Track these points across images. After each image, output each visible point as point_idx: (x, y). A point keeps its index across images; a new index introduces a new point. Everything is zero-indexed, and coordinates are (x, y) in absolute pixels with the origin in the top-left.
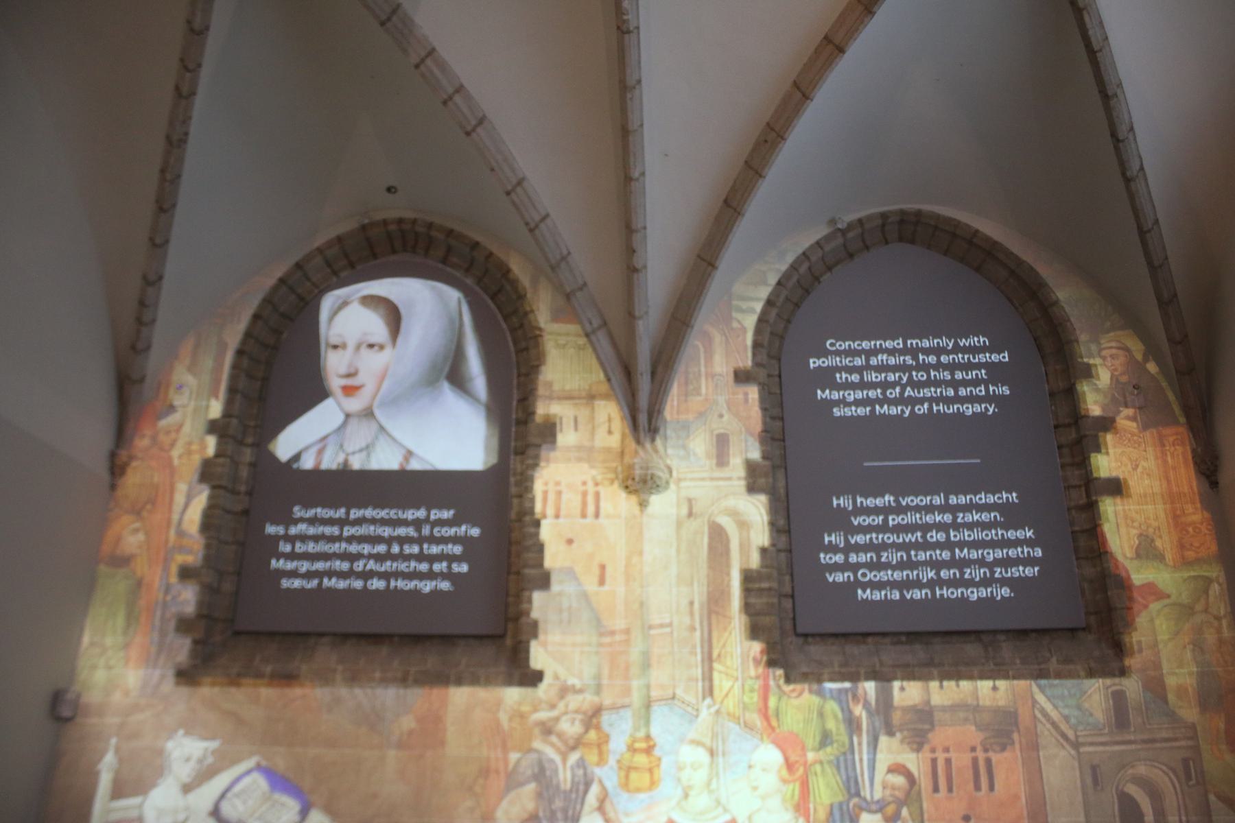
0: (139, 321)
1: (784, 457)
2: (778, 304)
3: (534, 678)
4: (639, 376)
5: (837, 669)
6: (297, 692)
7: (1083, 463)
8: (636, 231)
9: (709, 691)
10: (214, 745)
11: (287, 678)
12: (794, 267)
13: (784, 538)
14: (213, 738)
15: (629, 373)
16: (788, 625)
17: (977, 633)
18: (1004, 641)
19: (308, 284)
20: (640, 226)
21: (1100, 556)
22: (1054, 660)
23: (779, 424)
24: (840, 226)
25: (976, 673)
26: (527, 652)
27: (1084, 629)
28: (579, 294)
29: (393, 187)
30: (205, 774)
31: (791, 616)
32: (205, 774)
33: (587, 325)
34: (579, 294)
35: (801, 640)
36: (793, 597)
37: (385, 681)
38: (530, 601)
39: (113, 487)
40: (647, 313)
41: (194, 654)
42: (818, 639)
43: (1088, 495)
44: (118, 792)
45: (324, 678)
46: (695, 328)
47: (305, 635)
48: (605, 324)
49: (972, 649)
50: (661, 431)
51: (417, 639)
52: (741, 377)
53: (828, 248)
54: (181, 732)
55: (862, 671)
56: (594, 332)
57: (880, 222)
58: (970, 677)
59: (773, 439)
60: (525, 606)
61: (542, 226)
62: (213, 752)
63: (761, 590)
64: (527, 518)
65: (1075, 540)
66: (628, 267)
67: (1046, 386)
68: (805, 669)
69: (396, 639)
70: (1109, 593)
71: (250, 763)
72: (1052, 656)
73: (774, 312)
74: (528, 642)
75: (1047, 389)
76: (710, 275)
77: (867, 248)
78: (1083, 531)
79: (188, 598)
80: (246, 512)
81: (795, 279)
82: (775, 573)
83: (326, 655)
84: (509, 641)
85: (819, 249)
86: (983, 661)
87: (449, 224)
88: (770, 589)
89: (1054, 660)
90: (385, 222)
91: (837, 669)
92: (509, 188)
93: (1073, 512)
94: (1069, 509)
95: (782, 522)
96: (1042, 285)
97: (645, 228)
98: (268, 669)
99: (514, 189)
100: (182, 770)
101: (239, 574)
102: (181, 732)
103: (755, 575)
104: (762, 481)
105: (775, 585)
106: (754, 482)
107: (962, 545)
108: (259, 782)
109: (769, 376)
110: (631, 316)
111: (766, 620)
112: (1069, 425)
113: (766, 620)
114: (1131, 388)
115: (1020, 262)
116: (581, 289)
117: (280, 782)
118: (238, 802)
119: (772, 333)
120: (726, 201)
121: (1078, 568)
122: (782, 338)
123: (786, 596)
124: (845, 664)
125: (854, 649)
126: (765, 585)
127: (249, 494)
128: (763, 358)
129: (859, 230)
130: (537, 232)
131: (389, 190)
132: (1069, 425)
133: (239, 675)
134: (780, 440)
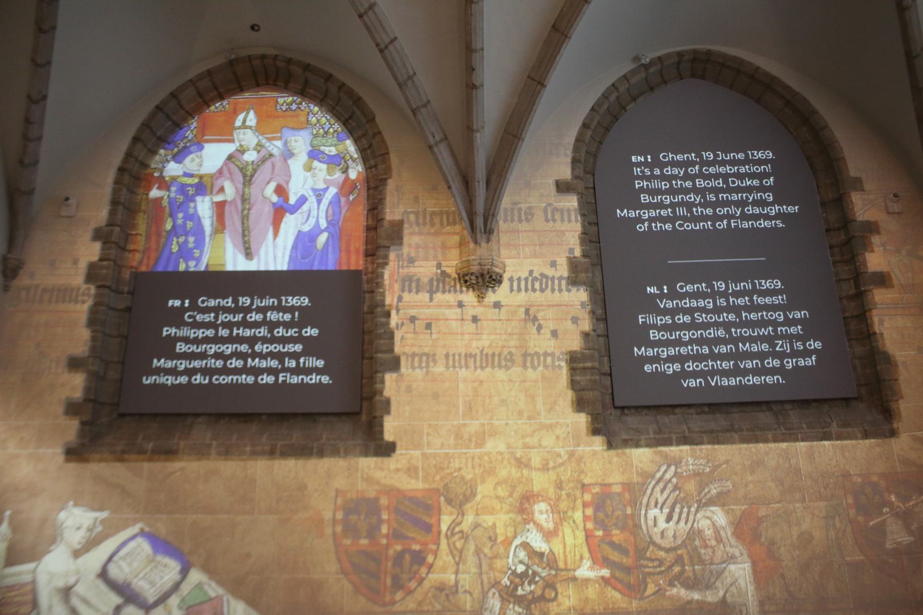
0: (26, 138)
2: (593, 127)
3: (387, 450)
4: (476, 183)
5: (652, 436)
6: (178, 465)
8: (476, 51)
10: (104, 515)
11: (170, 453)
12: (605, 96)
13: (602, 325)
14: (101, 509)
15: (467, 182)
16: (608, 398)
17: (767, 403)
18: (791, 410)
19: (183, 112)
20: (479, 46)
21: (869, 335)
22: (834, 423)
23: (594, 228)
24: (643, 62)
25: (770, 436)
26: (382, 426)
27: (856, 399)
28: (423, 110)
29: (258, 26)
30: (91, 544)
31: (610, 391)
32: (91, 544)
33: (431, 138)
34: (423, 110)
35: (619, 412)
36: (611, 375)
37: (254, 454)
38: (383, 382)
40: (483, 127)
41: (82, 434)
42: (633, 411)
43: (857, 286)
45: (201, 452)
46: (527, 139)
47: (186, 415)
48: (446, 138)
49: (764, 417)
50: (496, 231)
51: (283, 417)
52: (562, 187)
53: (633, 81)
54: (71, 503)
56: (436, 144)
58: (766, 441)
59: (591, 241)
60: (378, 386)
61: (391, 47)
62: (103, 522)
63: (584, 369)
66: (467, 85)
67: (818, 196)
68: (625, 436)
69: (264, 417)
70: (878, 368)
71: (135, 529)
72: (833, 422)
73: (589, 133)
74: (382, 417)
75: (818, 199)
76: (539, 92)
77: (665, 82)
78: (853, 317)
80: (128, 309)
81: (606, 106)
82: (596, 354)
83: (202, 433)
84: (364, 418)
85: (626, 81)
86: (776, 426)
88: (592, 368)
89: (834, 423)
90: (250, 58)
91: (652, 436)
92: (362, 11)
93: (844, 301)
96: (814, 112)
97: (482, 49)
98: (150, 446)
99: (366, 13)
100: (76, 538)
102: (71, 503)
103: (579, 356)
104: (582, 276)
105: (596, 364)
106: (576, 277)
107: (744, 340)
108: (145, 547)
109: (586, 188)
110: (469, 130)
111: (589, 395)
112: (839, 229)
113: (589, 395)
114: (891, 196)
115: (795, 94)
116: (425, 106)
117: (161, 545)
118: (123, 564)
119: (587, 152)
120: (554, 26)
121: (849, 347)
122: (595, 156)
123: (605, 374)
124: (659, 431)
125: (665, 419)
126: (589, 365)
127: (131, 293)
128: (580, 172)
129: (659, 66)
130: (386, 52)
131: (253, 28)
132: (839, 229)
133: (123, 452)
134: (597, 242)
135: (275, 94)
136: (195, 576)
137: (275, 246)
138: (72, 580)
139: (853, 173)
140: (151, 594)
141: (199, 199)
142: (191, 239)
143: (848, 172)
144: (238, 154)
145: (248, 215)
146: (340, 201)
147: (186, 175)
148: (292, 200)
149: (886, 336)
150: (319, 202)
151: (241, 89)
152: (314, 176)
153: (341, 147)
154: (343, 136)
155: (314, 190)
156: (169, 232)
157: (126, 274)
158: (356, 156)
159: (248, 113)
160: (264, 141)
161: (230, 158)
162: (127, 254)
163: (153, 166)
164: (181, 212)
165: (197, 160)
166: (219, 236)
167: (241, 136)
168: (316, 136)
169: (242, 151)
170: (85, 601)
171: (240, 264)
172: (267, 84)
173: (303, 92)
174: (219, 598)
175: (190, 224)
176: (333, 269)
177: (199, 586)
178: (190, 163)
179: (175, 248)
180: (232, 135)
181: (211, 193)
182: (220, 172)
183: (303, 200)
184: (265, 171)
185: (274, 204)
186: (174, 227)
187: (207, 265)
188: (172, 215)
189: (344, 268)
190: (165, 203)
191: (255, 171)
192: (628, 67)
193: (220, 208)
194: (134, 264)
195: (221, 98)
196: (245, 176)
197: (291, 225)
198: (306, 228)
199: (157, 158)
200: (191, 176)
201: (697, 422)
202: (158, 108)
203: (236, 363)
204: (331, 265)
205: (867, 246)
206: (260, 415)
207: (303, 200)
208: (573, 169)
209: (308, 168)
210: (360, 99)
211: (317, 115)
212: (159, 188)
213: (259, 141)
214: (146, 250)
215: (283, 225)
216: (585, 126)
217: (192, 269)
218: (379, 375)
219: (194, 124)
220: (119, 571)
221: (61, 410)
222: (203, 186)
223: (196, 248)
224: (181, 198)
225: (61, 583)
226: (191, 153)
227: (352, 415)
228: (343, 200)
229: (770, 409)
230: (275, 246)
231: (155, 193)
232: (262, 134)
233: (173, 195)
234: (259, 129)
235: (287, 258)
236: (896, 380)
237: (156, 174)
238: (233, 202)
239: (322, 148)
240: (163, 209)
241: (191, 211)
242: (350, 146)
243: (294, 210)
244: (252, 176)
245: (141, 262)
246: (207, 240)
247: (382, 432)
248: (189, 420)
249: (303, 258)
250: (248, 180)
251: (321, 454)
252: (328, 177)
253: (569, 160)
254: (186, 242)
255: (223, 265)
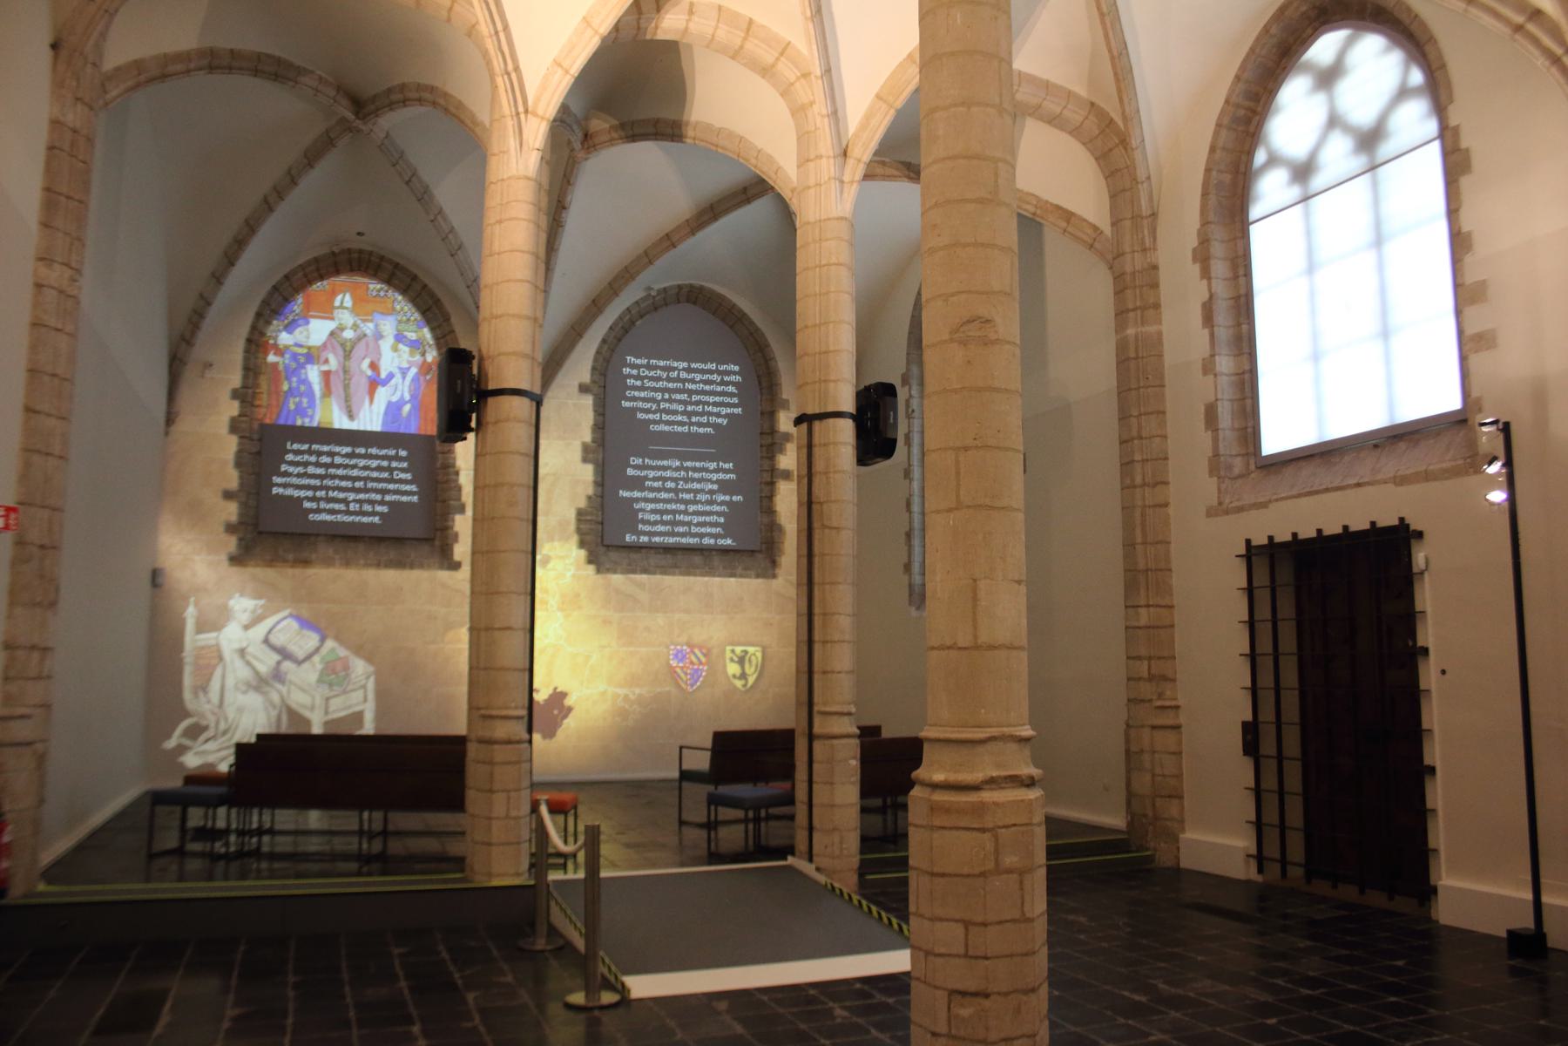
1: (603, 439)
6: (311, 571)
7: (772, 458)
9: (985, 855)
10: (262, 602)
11: (306, 563)
12: (620, 318)
14: (260, 598)
16: (599, 540)
30: (256, 620)
32: (256, 620)
36: (602, 524)
37: (367, 565)
38: (453, 520)
39: (167, 434)
44: (201, 628)
45: (328, 562)
47: (309, 535)
49: (697, 559)
52: (583, 389)
53: (643, 306)
55: (638, 568)
57: (677, 290)
58: (695, 575)
59: (599, 428)
60: (450, 523)
62: (261, 606)
64: (451, 470)
65: (761, 501)
68: (608, 566)
73: (606, 347)
78: (766, 497)
79: (231, 511)
80: (259, 453)
83: (325, 549)
84: (437, 543)
87: (397, 259)
89: (740, 568)
90: (349, 251)
93: (763, 486)
94: (761, 483)
95: (599, 479)
96: (768, 345)
100: (245, 618)
101: (258, 494)
102: (237, 595)
104: (591, 456)
108: (294, 625)
112: (768, 434)
113: (588, 538)
115: (758, 329)
117: (305, 623)
120: (594, 301)
124: (629, 565)
125: (634, 556)
126: (589, 518)
127: (260, 440)
133: (272, 561)
135: (366, 280)
136: (330, 644)
137: (371, 411)
138: (244, 645)
139: (784, 396)
140: (301, 654)
141: (309, 367)
142: (305, 401)
143: (781, 394)
144: (338, 331)
145: (349, 384)
146: (419, 379)
147: (297, 345)
148: (383, 375)
149: (783, 514)
150: (404, 378)
151: (337, 272)
152: (400, 356)
153: (420, 334)
154: (421, 324)
155: (400, 369)
156: (286, 392)
157: (256, 426)
158: (431, 342)
159: (344, 296)
160: (359, 322)
161: (332, 334)
162: (254, 409)
163: (269, 334)
164: (295, 376)
165: (305, 333)
166: (327, 399)
167: (340, 316)
168: (400, 322)
169: (341, 329)
170: (256, 658)
171: (340, 422)
172: (359, 270)
173: (389, 282)
174: (346, 658)
175: (303, 388)
176: (417, 432)
177: (333, 650)
178: (299, 335)
179: (292, 407)
180: (332, 313)
181: (318, 363)
182: (324, 346)
183: (391, 376)
184: (361, 347)
185: (369, 377)
186: (290, 388)
187: (319, 423)
188: (288, 378)
189: (423, 433)
190: (281, 367)
191: (353, 347)
192: (643, 294)
193: (326, 375)
194: (260, 417)
195: (322, 278)
196: (345, 351)
197: (383, 395)
198: (395, 399)
199: (272, 328)
200: (301, 346)
201: (654, 559)
202: (275, 288)
203: (368, 508)
204: (413, 430)
205: (782, 451)
206: (363, 537)
207: (391, 376)
208: (592, 375)
209: (395, 349)
210: (439, 300)
211: (400, 302)
212: (275, 354)
213: (355, 322)
214: (269, 406)
215: (376, 395)
216: (604, 341)
217: (307, 425)
218: (451, 516)
219: (300, 299)
220: (279, 639)
221: (222, 529)
222: (311, 356)
223: (309, 407)
224: (294, 365)
225: (237, 646)
226: (299, 326)
227: (428, 540)
228: (422, 378)
229: (703, 555)
230: (371, 411)
231: (272, 358)
232: (357, 315)
233: (287, 361)
234: (355, 310)
235: (380, 422)
236: (783, 543)
237: (271, 342)
238: (337, 372)
239: (406, 333)
240: (279, 372)
241: (303, 377)
242: (427, 334)
243: (385, 383)
244: (351, 352)
245: (265, 415)
246: (318, 402)
247: (452, 554)
248: (312, 539)
249: (393, 423)
250: (348, 355)
251: (412, 567)
252: (411, 359)
253: (589, 367)
254: (301, 402)
255: (332, 423)
